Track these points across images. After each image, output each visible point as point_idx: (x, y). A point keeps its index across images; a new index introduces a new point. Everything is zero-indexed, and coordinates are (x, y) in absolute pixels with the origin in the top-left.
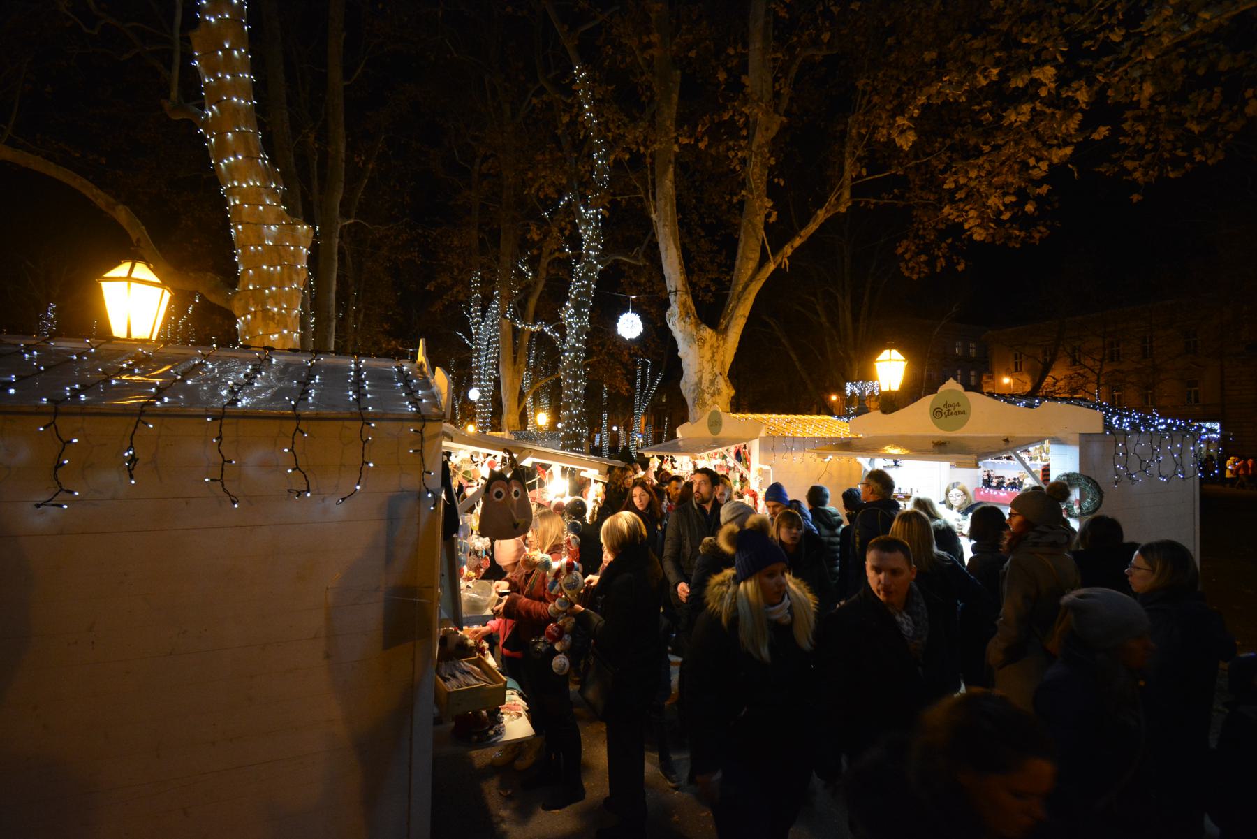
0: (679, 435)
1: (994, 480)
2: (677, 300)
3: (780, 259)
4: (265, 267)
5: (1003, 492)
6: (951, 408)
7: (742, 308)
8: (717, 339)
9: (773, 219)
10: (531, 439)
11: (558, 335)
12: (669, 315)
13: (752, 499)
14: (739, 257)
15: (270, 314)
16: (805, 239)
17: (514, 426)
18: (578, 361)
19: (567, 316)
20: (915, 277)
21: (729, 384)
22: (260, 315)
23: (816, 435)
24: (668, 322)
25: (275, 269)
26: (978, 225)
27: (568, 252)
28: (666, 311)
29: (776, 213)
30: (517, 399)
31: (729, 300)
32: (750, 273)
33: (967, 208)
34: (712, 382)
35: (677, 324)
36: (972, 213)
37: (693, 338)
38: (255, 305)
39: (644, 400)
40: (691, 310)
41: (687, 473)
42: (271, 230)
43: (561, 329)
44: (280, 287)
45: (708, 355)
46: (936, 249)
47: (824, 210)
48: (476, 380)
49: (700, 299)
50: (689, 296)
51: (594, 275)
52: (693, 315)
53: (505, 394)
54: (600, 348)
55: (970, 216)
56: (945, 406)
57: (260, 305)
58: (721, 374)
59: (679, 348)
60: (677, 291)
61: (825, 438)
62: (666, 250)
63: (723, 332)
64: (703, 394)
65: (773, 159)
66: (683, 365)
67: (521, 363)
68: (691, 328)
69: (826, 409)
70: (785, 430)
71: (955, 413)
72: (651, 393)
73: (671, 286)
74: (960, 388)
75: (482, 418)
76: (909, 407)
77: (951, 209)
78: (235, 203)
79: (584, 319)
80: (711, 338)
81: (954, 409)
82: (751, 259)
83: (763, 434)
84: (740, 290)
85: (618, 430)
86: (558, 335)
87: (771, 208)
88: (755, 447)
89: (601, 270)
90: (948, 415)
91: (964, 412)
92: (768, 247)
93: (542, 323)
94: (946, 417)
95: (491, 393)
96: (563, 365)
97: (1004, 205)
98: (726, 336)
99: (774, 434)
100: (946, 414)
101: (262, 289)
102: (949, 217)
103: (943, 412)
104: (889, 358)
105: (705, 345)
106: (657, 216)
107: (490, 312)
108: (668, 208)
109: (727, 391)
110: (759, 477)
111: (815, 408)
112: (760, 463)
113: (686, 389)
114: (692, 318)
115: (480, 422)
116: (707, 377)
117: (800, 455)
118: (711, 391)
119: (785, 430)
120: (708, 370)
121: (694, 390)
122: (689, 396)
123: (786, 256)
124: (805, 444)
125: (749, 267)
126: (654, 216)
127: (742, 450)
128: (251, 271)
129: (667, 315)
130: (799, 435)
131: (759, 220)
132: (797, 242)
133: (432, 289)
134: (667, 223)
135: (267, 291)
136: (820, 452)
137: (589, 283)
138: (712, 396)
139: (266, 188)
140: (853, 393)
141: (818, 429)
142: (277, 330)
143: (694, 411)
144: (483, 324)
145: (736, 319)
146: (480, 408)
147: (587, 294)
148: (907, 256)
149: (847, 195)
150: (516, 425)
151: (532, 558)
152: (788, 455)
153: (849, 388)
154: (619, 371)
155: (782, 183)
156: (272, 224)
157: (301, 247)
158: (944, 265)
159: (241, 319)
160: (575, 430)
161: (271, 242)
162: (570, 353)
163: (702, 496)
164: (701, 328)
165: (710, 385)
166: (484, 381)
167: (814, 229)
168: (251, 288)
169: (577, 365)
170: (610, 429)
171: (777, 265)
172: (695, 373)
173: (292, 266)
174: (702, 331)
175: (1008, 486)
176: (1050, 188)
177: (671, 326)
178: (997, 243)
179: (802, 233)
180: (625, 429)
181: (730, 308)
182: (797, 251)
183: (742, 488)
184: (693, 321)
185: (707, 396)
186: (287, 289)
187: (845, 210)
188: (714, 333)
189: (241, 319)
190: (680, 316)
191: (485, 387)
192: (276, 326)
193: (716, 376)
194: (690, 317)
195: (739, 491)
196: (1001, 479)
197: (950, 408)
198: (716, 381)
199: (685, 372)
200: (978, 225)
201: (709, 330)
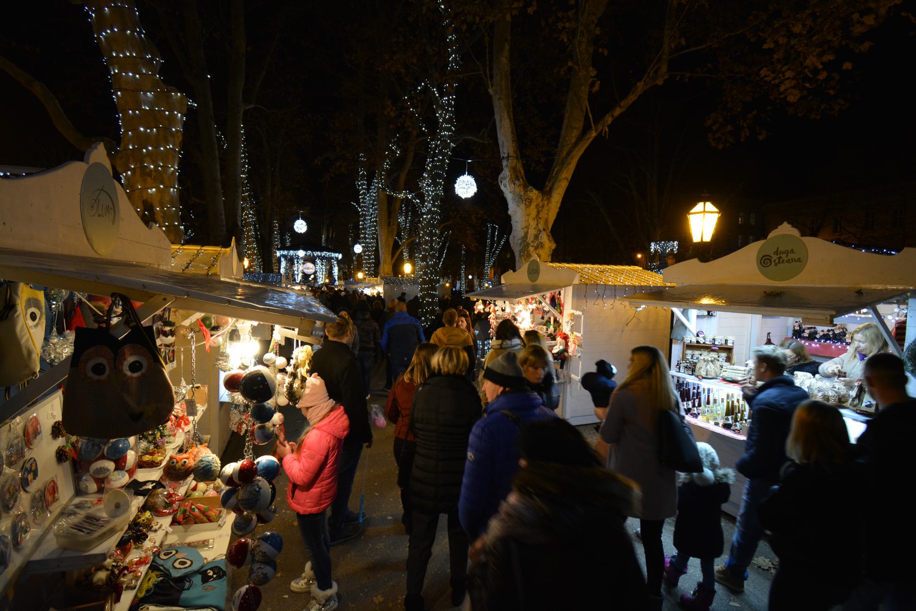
0: (503, 281)
1: (806, 331)
2: (509, 164)
3: (601, 127)
4: (142, 129)
5: (816, 344)
6: (784, 256)
7: (565, 171)
8: (542, 200)
9: (596, 88)
10: (397, 283)
11: (419, 201)
12: (502, 178)
13: (563, 341)
14: (564, 126)
15: (148, 170)
16: (624, 109)
17: (388, 274)
18: (434, 222)
19: (425, 185)
20: (720, 147)
21: (551, 238)
22: (138, 172)
23: (627, 283)
24: (500, 184)
25: (152, 130)
26: (794, 87)
27: (425, 131)
28: (499, 174)
29: (599, 82)
30: (390, 253)
31: (554, 165)
32: (574, 140)
33: (785, 68)
34: (536, 237)
35: (508, 186)
36: (789, 74)
37: (521, 198)
38: (135, 163)
39: (492, 256)
40: (520, 173)
41: (509, 315)
42: (148, 96)
43: (421, 196)
44: (156, 147)
45: (533, 212)
46: (742, 121)
47: (642, 83)
48: (363, 238)
49: (532, 169)
50: (519, 162)
51: (448, 152)
52: (522, 178)
53: (382, 249)
54: (455, 213)
55: (786, 77)
56: (776, 253)
57: (138, 163)
58: (544, 230)
59: (509, 207)
60: (508, 156)
61: (635, 286)
62: (501, 121)
63: (546, 193)
64: (528, 247)
65: (598, 28)
66: (513, 222)
67: (394, 224)
68: (519, 190)
69: (633, 262)
70: (597, 278)
71: (788, 261)
72: (498, 251)
73: (504, 153)
74: (795, 232)
75: (367, 267)
76: (719, 259)
77: (768, 70)
78: (114, 72)
79: (439, 188)
80: (537, 198)
81: (787, 256)
82: (575, 128)
83: (576, 281)
84: (564, 155)
85: (473, 278)
86: (419, 201)
87: (595, 77)
88: (567, 297)
89: (454, 147)
90: (779, 263)
91: (799, 260)
92: (590, 116)
93: (406, 192)
94: (776, 265)
95: (374, 248)
96: (422, 225)
97: (822, 63)
98: (551, 197)
99: (587, 282)
100: (777, 262)
101: (140, 149)
102: (766, 79)
103: (773, 260)
104: (706, 210)
105: (532, 204)
106: (493, 90)
107: (374, 185)
108: (503, 83)
109: (549, 245)
110: (571, 321)
111: (624, 262)
112: (572, 309)
113: (514, 243)
114: (521, 180)
115: (366, 271)
116: (532, 232)
117: (611, 301)
118: (535, 245)
119: (597, 278)
120: (533, 227)
121: (521, 244)
122: (516, 249)
123: (607, 124)
124: (616, 291)
125: (573, 135)
126: (491, 91)
127: (557, 296)
128: (130, 133)
129: (499, 178)
130: (610, 283)
131: (584, 91)
132: (617, 112)
133: (319, 163)
134: (502, 96)
135: (144, 150)
136: (633, 300)
137: (443, 158)
138: (536, 249)
139: (142, 58)
140: (656, 251)
141: (628, 278)
142: (155, 185)
143: (520, 261)
144: (368, 195)
145: (560, 181)
146: (366, 259)
147: (442, 167)
148: (714, 128)
149: (664, 68)
150: (390, 273)
151: (180, 464)
152: (600, 301)
153: (653, 246)
154: (469, 232)
155: (606, 53)
156: (148, 92)
157: (176, 113)
158: (748, 134)
159: (123, 175)
160: (431, 277)
161: (148, 107)
162: (427, 215)
163: (333, 436)
164: (529, 189)
165: (534, 239)
166: (370, 239)
167: (633, 100)
168: (131, 147)
169: (433, 226)
170: (467, 277)
171: (597, 133)
172: (522, 229)
173: (167, 129)
174: (529, 192)
175: (821, 337)
176: (872, 44)
177: (502, 187)
178: (800, 115)
179: (622, 104)
180: (478, 278)
181: (555, 172)
182: (616, 120)
183: (555, 331)
184: (522, 183)
185: (531, 249)
186: (162, 149)
187: (662, 83)
188: (540, 194)
189: (123, 175)
190: (510, 179)
191: (370, 243)
192: (153, 181)
193: (540, 231)
194: (519, 180)
195: (552, 333)
196: (813, 330)
197: (782, 256)
198: (540, 235)
199: (514, 228)
200: (794, 87)
201: (535, 192)
